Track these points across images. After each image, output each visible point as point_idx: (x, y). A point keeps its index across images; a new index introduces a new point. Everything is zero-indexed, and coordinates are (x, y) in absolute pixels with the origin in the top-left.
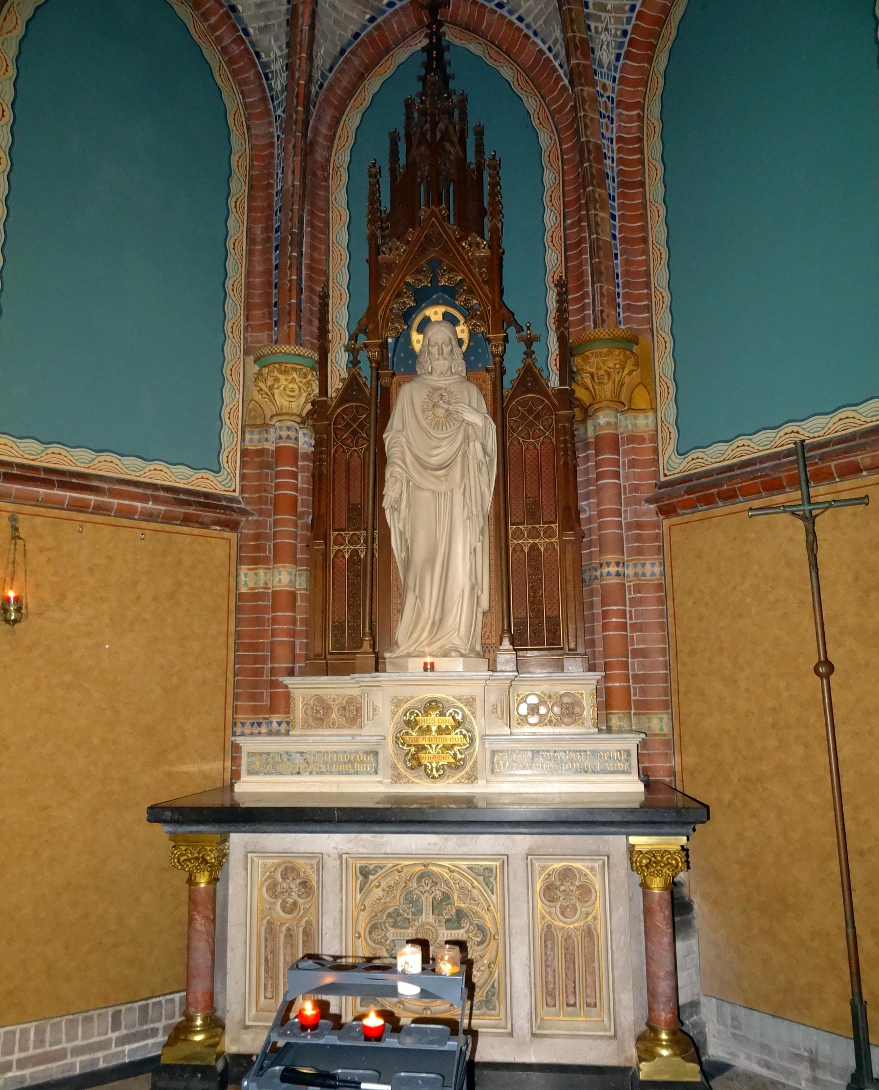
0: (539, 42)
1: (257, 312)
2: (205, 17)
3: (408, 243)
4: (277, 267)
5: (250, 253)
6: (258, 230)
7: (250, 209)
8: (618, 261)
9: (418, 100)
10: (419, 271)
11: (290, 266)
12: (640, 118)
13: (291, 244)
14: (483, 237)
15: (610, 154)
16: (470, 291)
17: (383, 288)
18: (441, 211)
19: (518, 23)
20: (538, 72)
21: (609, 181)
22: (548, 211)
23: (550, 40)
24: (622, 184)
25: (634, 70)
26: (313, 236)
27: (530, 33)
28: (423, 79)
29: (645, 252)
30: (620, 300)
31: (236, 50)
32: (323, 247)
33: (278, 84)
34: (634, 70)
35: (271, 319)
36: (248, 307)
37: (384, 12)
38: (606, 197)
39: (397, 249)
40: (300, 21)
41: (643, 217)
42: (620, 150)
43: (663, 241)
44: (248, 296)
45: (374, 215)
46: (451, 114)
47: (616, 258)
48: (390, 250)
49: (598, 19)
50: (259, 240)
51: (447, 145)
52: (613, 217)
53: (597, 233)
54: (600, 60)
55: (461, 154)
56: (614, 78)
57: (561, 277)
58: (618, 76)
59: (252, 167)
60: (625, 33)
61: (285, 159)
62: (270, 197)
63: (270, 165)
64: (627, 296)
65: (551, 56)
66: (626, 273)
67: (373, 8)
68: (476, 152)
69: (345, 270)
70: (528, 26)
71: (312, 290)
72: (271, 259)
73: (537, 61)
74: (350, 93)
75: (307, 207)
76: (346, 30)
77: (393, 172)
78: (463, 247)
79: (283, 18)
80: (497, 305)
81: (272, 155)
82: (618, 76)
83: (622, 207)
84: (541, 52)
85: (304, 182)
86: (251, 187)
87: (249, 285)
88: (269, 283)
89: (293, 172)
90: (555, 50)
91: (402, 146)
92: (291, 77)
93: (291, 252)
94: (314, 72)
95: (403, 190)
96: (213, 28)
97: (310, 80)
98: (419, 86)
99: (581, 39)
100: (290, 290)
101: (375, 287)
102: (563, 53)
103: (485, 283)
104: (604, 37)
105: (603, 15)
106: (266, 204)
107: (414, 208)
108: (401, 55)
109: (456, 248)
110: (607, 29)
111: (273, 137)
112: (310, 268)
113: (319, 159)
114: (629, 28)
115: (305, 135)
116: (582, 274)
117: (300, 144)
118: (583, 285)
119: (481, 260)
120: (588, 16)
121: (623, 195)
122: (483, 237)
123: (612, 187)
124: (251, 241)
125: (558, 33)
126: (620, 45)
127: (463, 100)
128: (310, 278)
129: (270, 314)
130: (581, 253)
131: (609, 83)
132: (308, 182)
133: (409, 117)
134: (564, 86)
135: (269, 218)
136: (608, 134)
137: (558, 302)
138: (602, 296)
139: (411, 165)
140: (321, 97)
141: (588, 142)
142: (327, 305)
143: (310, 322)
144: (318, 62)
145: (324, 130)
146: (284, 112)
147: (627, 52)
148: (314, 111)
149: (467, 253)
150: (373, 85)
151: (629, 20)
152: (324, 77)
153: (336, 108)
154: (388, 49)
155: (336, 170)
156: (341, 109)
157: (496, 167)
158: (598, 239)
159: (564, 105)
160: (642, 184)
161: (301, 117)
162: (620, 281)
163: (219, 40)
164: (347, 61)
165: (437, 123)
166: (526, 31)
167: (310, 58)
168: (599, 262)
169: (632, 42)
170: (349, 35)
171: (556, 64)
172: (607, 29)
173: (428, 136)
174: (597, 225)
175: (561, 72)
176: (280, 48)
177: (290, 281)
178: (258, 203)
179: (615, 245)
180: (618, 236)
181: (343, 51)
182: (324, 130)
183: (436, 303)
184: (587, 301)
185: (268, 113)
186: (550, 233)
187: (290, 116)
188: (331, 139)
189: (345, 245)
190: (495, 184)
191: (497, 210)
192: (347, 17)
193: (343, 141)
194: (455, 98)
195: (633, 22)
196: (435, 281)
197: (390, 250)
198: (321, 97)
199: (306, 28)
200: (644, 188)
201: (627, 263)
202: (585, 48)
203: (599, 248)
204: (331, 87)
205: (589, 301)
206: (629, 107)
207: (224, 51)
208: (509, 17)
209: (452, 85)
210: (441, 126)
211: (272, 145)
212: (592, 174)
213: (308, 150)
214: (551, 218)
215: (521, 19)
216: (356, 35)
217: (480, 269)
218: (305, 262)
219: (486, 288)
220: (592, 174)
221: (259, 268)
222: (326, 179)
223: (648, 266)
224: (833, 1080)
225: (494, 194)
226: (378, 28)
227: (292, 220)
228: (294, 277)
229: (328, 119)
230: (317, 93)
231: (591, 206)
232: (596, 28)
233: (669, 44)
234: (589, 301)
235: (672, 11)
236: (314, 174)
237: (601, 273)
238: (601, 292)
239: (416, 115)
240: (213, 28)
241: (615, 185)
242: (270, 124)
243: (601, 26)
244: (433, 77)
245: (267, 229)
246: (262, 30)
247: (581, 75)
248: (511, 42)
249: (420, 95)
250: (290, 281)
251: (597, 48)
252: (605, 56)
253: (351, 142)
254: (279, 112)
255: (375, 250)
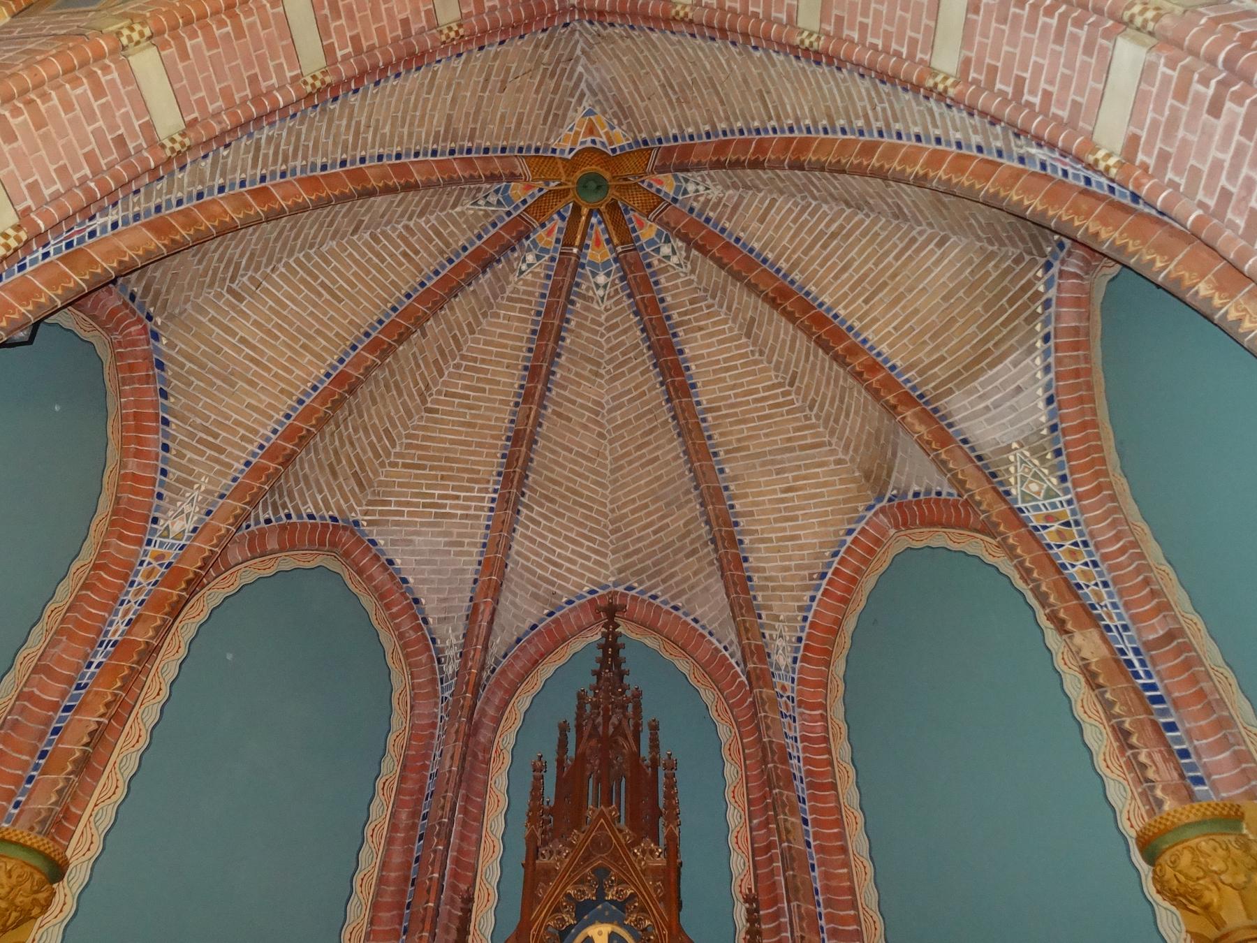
0: (714, 641)
1: (385, 915)
2: (388, 607)
3: (571, 845)
4: (417, 860)
5: (390, 841)
6: (404, 815)
7: (399, 792)
8: (816, 874)
9: (591, 694)
10: (582, 881)
11: (439, 833)
12: (824, 718)
13: (438, 835)
14: (657, 843)
15: (795, 754)
16: (643, 910)
17: (539, 900)
18: (610, 812)
19: (693, 624)
20: (715, 668)
21: (797, 783)
22: (730, 808)
23: (726, 640)
24: (811, 785)
25: (813, 673)
26: (464, 824)
27: (706, 634)
28: (597, 674)
29: (846, 864)
30: (822, 923)
31: (413, 635)
32: (474, 836)
33: (450, 669)
34: (813, 673)
35: (401, 924)
36: (375, 906)
37: (563, 608)
38: (795, 800)
39: (559, 853)
40: (480, 617)
41: (839, 823)
42: (805, 749)
43: (866, 853)
44: (378, 894)
45: (536, 812)
46: (625, 708)
47: (813, 870)
48: (551, 853)
49: (773, 628)
50: (402, 826)
51: (621, 740)
52: (805, 822)
53: (789, 841)
54: (777, 664)
55: (635, 749)
56: (793, 680)
57: (750, 890)
58: (798, 735)
59: (408, 747)
60: (799, 640)
61: (445, 743)
62: (422, 781)
63: (429, 747)
64: (831, 918)
65: (727, 654)
66: (827, 889)
67: (552, 605)
68: (651, 747)
69: (497, 866)
70: (703, 627)
71: (454, 888)
72: (412, 850)
73: (713, 657)
74: (523, 677)
75: (462, 792)
76: (524, 621)
77: (560, 762)
78: (635, 854)
79: (464, 613)
80: (674, 932)
81: (432, 736)
82: (796, 676)
83: (814, 810)
84: (716, 649)
85: (463, 767)
86: (404, 768)
87: (381, 881)
88: (406, 878)
89: (452, 758)
90: (730, 650)
91: (572, 736)
92: (464, 665)
93: (437, 844)
94: (488, 658)
95: (570, 782)
96: (393, 617)
97: (482, 668)
98: (594, 680)
99: (756, 645)
100: (428, 891)
101: (530, 899)
102: (739, 654)
103: (661, 899)
104: (779, 642)
105: (777, 624)
106: (417, 787)
107: (581, 806)
108: (577, 645)
109: (628, 858)
110: (781, 636)
111: (436, 717)
112: (457, 861)
113: (483, 740)
114: (804, 635)
115: (470, 718)
116: (774, 885)
117: (464, 728)
118: (775, 901)
119: (655, 870)
120: (762, 626)
121: (813, 798)
122: (657, 843)
123: (801, 788)
124: (393, 827)
125: (733, 637)
126: (797, 650)
127: (638, 695)
128: (455, 875)
129: (401, 916)
130: (771, 860)
131: (788, 684)
132: (467, 765)
133: (581, 707)
134: (742, 682)
135: (418, 802)
136: (791, 733)
137: (748, 921)
138: (801, 918)
139: (581, 759)
140: (492, 680)
141: (771, 742)
142: (470, 911)
143: (447, 930)
144: (494, 650)
145: (491, 712)
146: (452, 695)
147: (804, 656)
148: (483, 694)
149: (639, 862)
150: (546, 670)
151: (802, 629)
152: (497, 662)
153: (506, 691)
154: (564, 640)
155: (499, 753)
156: (511, 692)
157: (671, 766)
158: (790, 848)
159: (743, 700)
160: (834, 786)
161: (468, 703)
162: (821, 898)
163: (397, 627)
164: (522, 649)
165: (610, 718)
166: (701, 630)
167: (486, 648)
168: (794, 876)
169: (807, 647)
170: (526, 626)
171: (733, 661)
172: (781, 636)
173: (600, 729)
174: (788, 832)
175: (738, 669)
176: (457, 638)
177: (431, 879)
178: (409, 785)
179: (811, 854)
180: (813, 844)
181: (519, 640)
182: (491, 712)
183: (604, 921)
184: (782, 920)
185: (435, 694)
186: (735, 834)
187: (456, 702)
188: (497, 721)
189: (500, 835)
190: (671, 785)
191: (673, 816)
192: (526, 611)
193: (510, 722)
194: (629, 694)
195: (807, 630)
196: (601, 895)
197: (551, 853)
198: (492, 680)
199: (484, 624)
200: (836, 790)
201: (827, 876)
202: (763, 654)
203: (793, 859)
204: (503, 672)
205: (785, 920)
206: (813, 707)
207: (401, 636)
208: (684, 618)
209: (626, 680)
210: (614, 720)
211: (434, 725)
212: (777, 775)
213: (473, 729)
214: (735, 817)
215: (696, 621)
216: (534, 627)
217: (654, 882)
218: (452, 854)
219: (661, 906)
220: (777, 775)
221: (397, 859)
222: (488, 763)
223: (852, 881)
224: (1231, 794)
225: (670, 796)
226: (557, 621)
227: (443, 808)
228: (436, 875)
229: (497, 701)
230: (488, 677)
231: (779, 810)
232: (771, 636)
233: (845, 652)
234: (785, 920)
235: (844, 623)
236: (475, 756)
237: (797, 890)
238: (799, 912)
239: (588, 707)
240: (393, 617)
241: (804, 786)
242: (436, 704)
243: (775, 634)
244: (607, 674)
245: (414, 814)
246: (441, 620)
247: (761, 678)
248: (688, 640)
249: (593, 688)
250: (431, 879)
251: (773, 652)
252: (782, 659)
253: (519, 724)
254: (447, 694)
255: (533, 853)
